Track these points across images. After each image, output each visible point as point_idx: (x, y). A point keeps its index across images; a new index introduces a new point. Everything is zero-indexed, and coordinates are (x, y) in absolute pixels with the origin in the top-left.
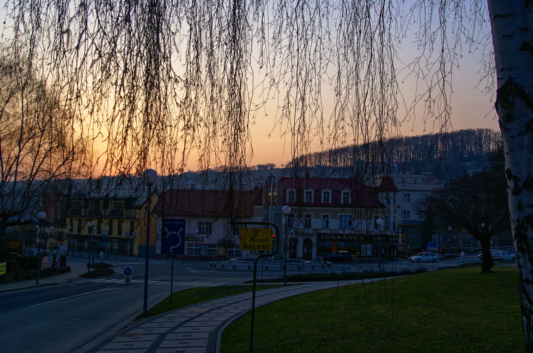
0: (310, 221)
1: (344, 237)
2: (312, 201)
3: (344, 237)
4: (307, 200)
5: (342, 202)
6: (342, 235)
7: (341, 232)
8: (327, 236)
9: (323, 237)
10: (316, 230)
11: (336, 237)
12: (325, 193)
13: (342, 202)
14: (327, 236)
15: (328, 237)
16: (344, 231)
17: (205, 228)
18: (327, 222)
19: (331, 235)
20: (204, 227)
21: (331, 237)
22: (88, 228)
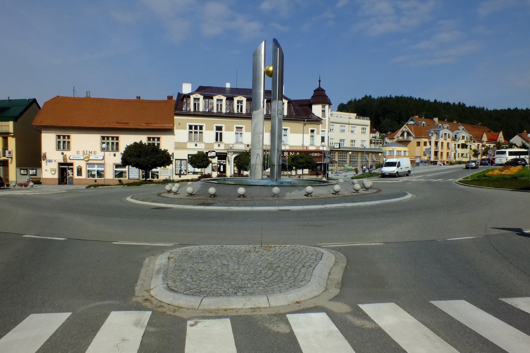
0: (221, 134)
17: (219, 133)
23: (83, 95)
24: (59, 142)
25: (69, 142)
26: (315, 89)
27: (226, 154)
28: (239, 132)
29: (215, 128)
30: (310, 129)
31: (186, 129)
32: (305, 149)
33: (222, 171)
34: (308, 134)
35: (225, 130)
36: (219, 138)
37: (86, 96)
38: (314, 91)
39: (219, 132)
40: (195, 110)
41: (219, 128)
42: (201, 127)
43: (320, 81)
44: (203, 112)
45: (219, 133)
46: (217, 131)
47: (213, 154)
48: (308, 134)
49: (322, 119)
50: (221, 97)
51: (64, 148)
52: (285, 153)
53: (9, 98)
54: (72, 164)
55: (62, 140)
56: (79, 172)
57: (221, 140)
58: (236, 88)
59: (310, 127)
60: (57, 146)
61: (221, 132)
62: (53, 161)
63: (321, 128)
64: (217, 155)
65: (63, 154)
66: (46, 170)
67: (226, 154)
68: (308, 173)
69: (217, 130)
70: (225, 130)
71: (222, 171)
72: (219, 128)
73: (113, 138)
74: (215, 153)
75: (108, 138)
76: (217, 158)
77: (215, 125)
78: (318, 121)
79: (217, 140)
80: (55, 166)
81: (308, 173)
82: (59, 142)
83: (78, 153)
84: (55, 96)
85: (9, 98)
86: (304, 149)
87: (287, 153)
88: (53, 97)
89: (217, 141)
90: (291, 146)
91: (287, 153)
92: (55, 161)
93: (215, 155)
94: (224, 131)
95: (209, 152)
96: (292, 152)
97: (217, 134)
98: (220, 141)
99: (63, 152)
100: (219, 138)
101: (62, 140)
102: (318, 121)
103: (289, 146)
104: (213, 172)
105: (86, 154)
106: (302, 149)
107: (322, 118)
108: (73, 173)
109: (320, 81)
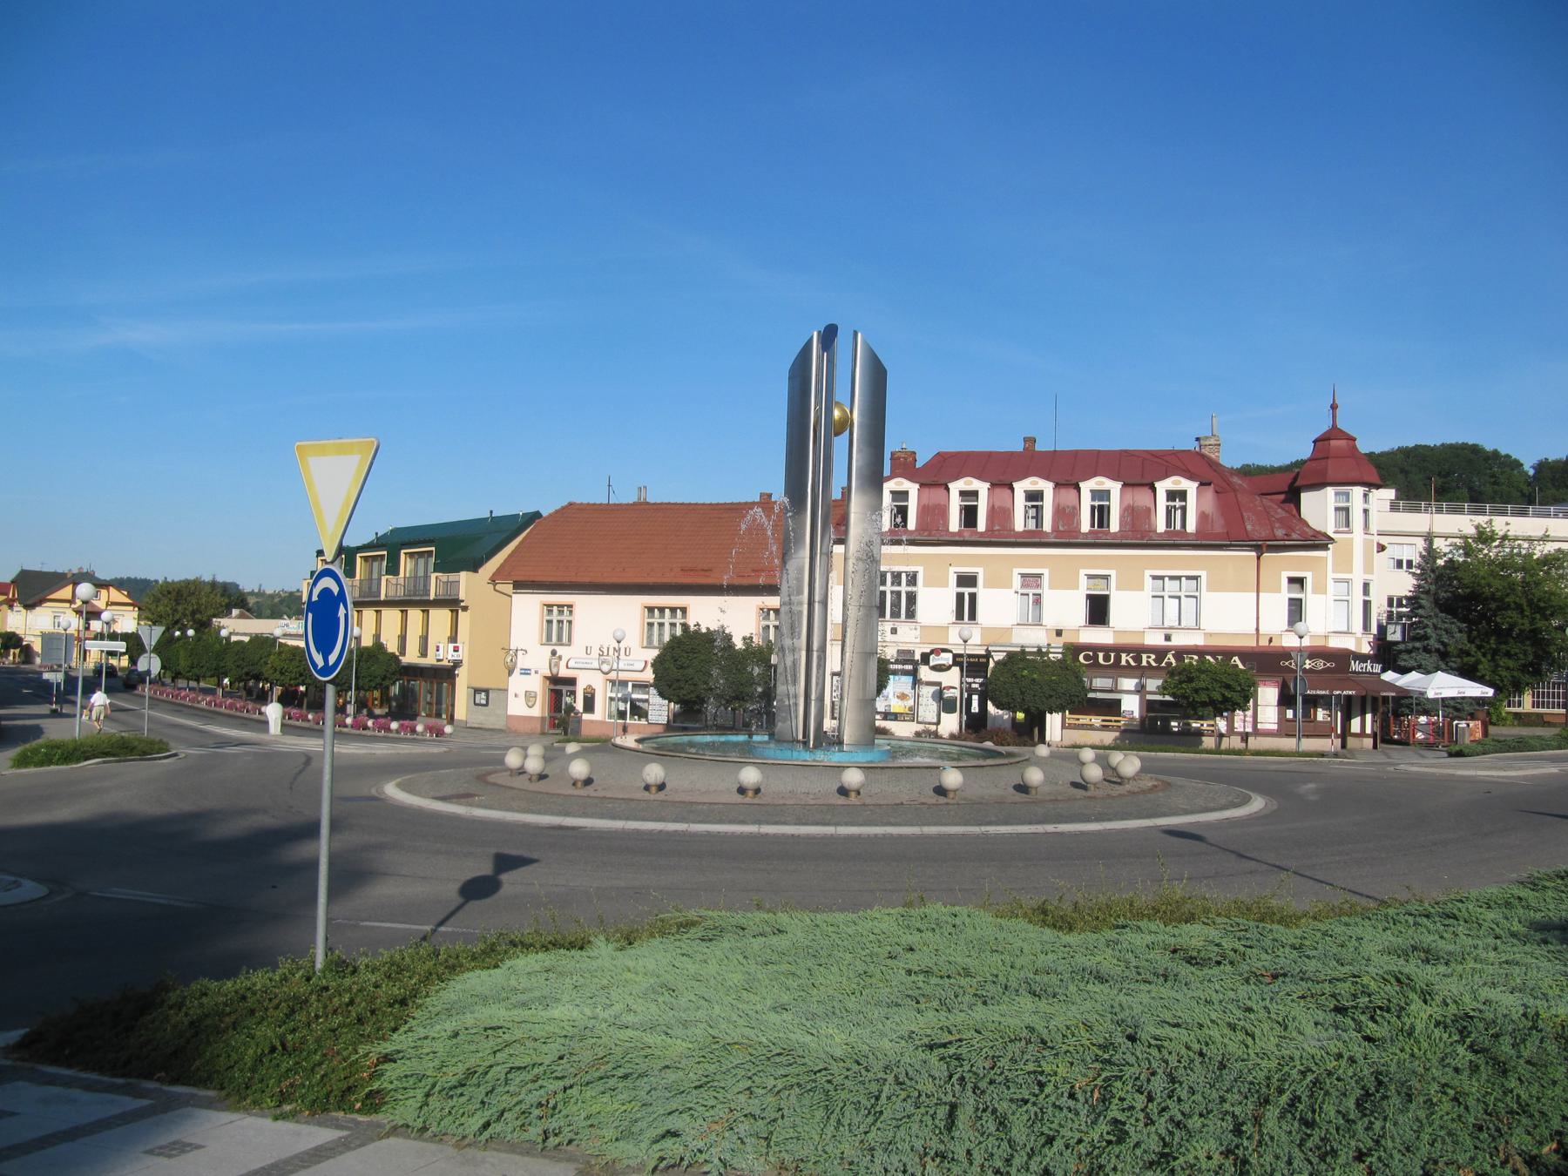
0: (973, 597)
1: (1170, 657)
2: (1047, 526)
3: (1170, 657)
4: (1168, 524)
5: (1161, 526)
6: (1160, 653)
7: (1156, 639)
8: (1101, 655)
9: (1086, 657)
10: (1059, 633)
11: (1138, 659)
12: (1172, 495)
13: (1161, 526)
14: (1101, 655)
15: (1107, 658)
16: (1168, 638)
17: (967, 598)
18: (1038, 600)
19: (1119, 650)
20: (899, 594)
21: (1118, 659)
22: (20, 569)
23: (630, 498)
24: (550, 622)
25: (570, 622)
26: (1316, 436)
27: (984, 660)
28: (1031, 591)
29: (953, 580)
30: (1285, 575)
31: (947, 586)
32: (1264, 642)
33: (977, 711)
34: (1279, 591)
35: (1051, 587)
36: (966, 609)
37: (636, 500)
38: (1315, 442)
39: (967, 591)
40: (1101, 525)
41: (967, 580)
42: (913, 579)
43: (1334, 407)
44: (1027, 533)
45: (967, 598)
46: (961, 590)
47: (945, 659)
48: (1279, 591)
49: (1332, 539)
50: (902, 483)
51: (560, 638)
52: (1144, 656)
53: (491, 512)
54: (572, 682)
55: (555, 617)
56: (589, 705)
57: (973, 616)
58: (1052, 449)
59: (1284, 565)
60: (544, 634)
61: (972, 590)
62: (533, 672)
63: (1333, 572)
64: (955, 663)
65: (554, 653)
66: (516, 696)
67: (984, 660)
68: (1275, 727)
69: (959, 585)
70: (1051, 587)
71: (977, 711)
72: (967, 580)
73: (673, 610)
74: (950, 655)
75: (662, 610)
76: (956, 670)
77: (952, 570)
78: (1319, 541)
79: (960, 616)
80: (536, 684)
81: (1275, 727)
82: (550, 622)
83: (588, 650)
84: (565, 503)
85: (491, 512)
86: (1260, 644)
87: (1153, 657)
88: (558, 507)
89: (884, 617)
90: (1211, 635)
91: (1153, 657)
92: (536, 672)
93: (951, 663)
94: (981, 591)
95: (932, 652)
96: (1214, 654)
97: (960, 597)
98: (969, 619)
99: (556, 648)
100: (966, 609)
101: (555, 617)
102: (1319, 541)
103: (1203, 636)
104: (943, 715)
105: (606, 653)
106: (1254, 644)
107: (1332, 536)
108: (1428, 745)
109: (1334, 407)
